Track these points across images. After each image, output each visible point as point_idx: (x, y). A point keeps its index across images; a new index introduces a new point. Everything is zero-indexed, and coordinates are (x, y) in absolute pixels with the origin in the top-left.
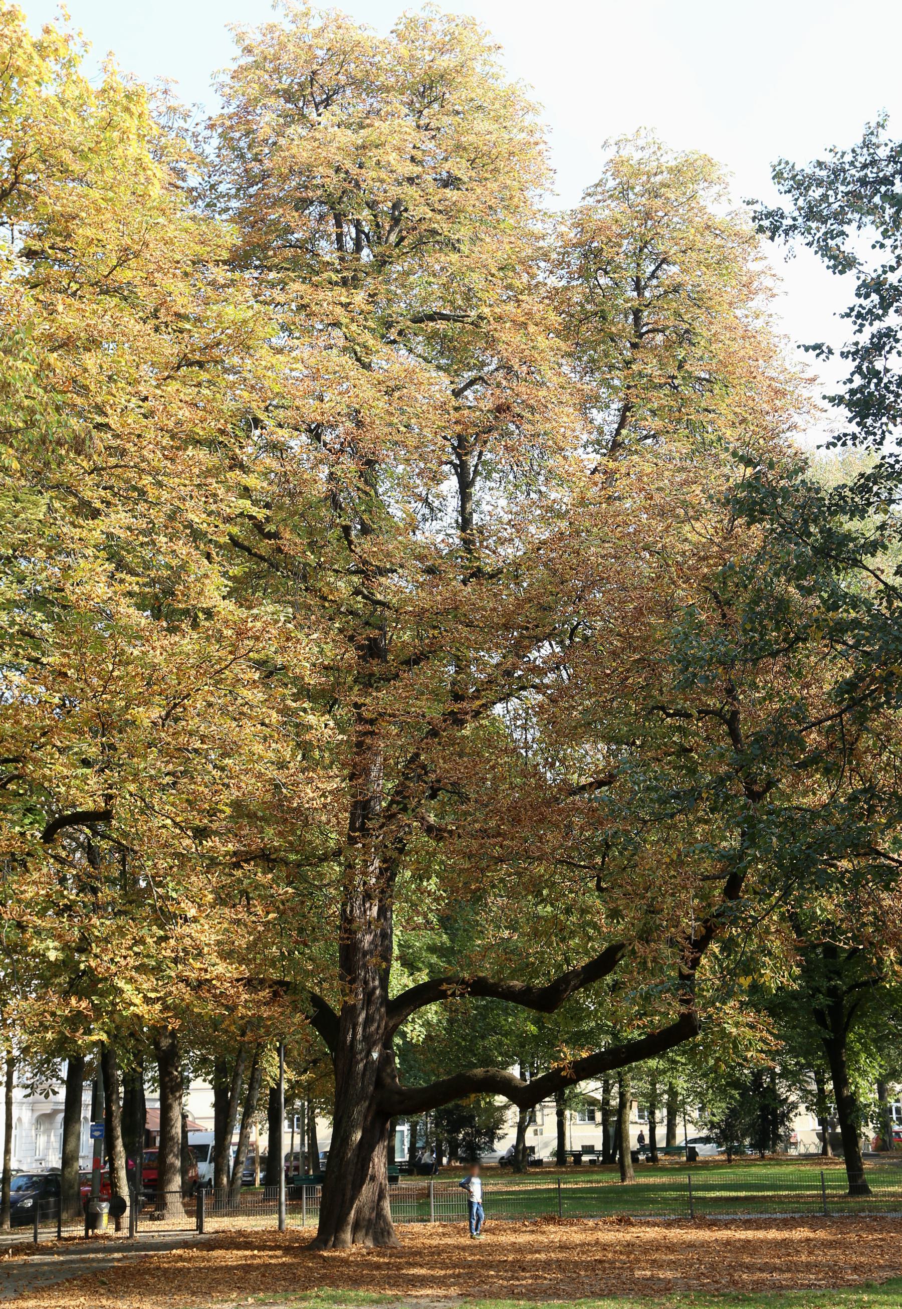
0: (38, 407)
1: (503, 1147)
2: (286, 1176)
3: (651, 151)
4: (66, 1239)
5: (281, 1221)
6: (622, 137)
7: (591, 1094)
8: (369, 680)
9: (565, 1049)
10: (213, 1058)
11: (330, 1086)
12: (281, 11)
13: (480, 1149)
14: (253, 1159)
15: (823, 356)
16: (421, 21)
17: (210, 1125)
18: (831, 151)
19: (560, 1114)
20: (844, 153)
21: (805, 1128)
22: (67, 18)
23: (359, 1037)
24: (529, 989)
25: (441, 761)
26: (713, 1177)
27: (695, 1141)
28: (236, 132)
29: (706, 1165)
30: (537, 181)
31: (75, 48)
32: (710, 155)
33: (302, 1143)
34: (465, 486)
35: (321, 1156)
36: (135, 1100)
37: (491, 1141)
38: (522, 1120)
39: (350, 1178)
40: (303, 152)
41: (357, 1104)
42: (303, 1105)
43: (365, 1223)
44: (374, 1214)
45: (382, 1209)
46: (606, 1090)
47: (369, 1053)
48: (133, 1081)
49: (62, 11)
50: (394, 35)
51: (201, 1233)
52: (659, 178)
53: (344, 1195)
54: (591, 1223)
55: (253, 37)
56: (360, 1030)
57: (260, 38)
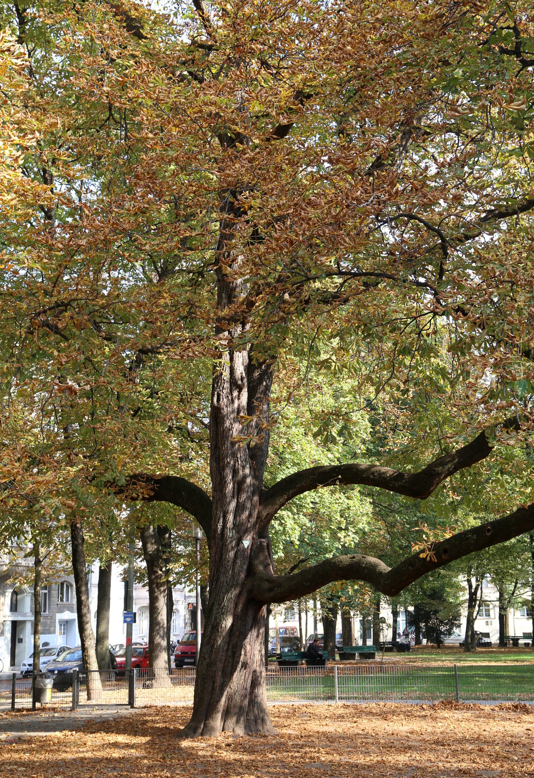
1: (460, 633)
4: (19, 710)
9: (426, 530)
23: (230, 525)
24: (400, 476)
39: (220, 665)
41: (228, 592)
43: (237, 710)
44: (246, 702)
45: (256, 697)
47: (239, 541)
53: (214, 683)
54: (487, 707)
56: (231, 517)
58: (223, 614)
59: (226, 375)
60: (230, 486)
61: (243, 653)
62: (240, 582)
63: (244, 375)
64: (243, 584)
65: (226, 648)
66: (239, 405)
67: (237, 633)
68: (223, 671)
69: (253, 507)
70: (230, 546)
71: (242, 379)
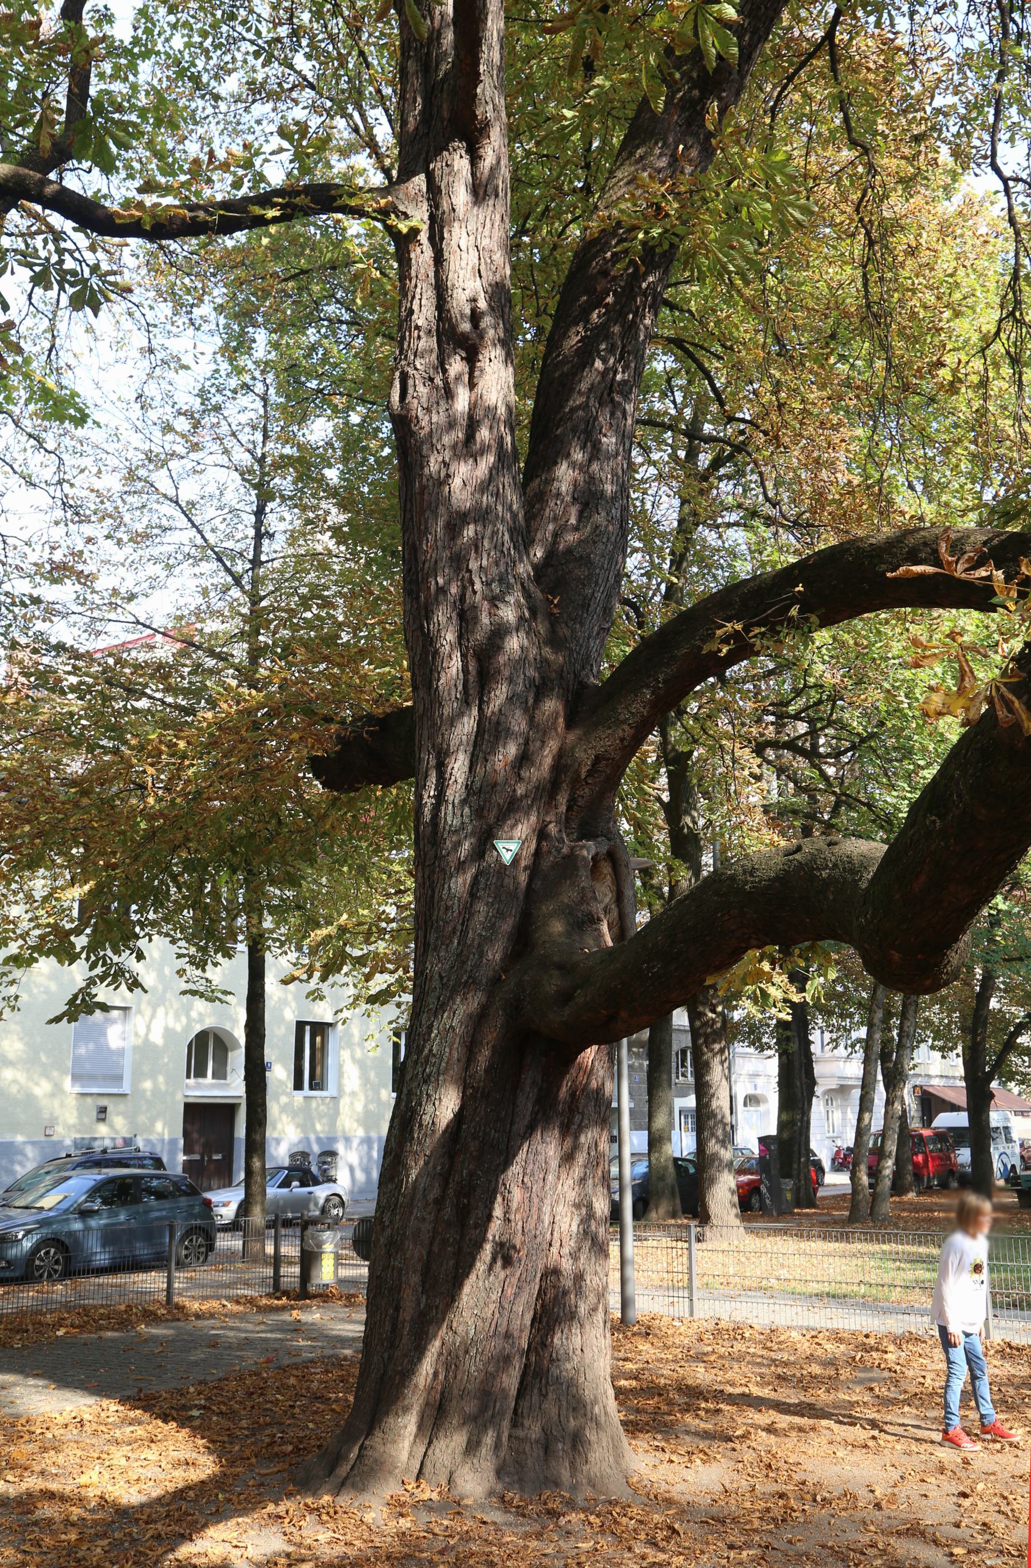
23: (455, 792)
43: (470, 1407)
44: (511, 1380)
47: (485, 840)
53: (397, 1309)
56: (459, 767)
58: (426, 1081)
59: (424, 314)
60: (454, 666)
61: (498, 1211)
62: (484, 974)
63: (482, 304)
64: (495, 982)
65: (434, 1193)
66: (473, 406)
67: (473, 1146)
68: (426, 1272)
69: (538, 730)
70: (452, 859)
71: (475, 317)
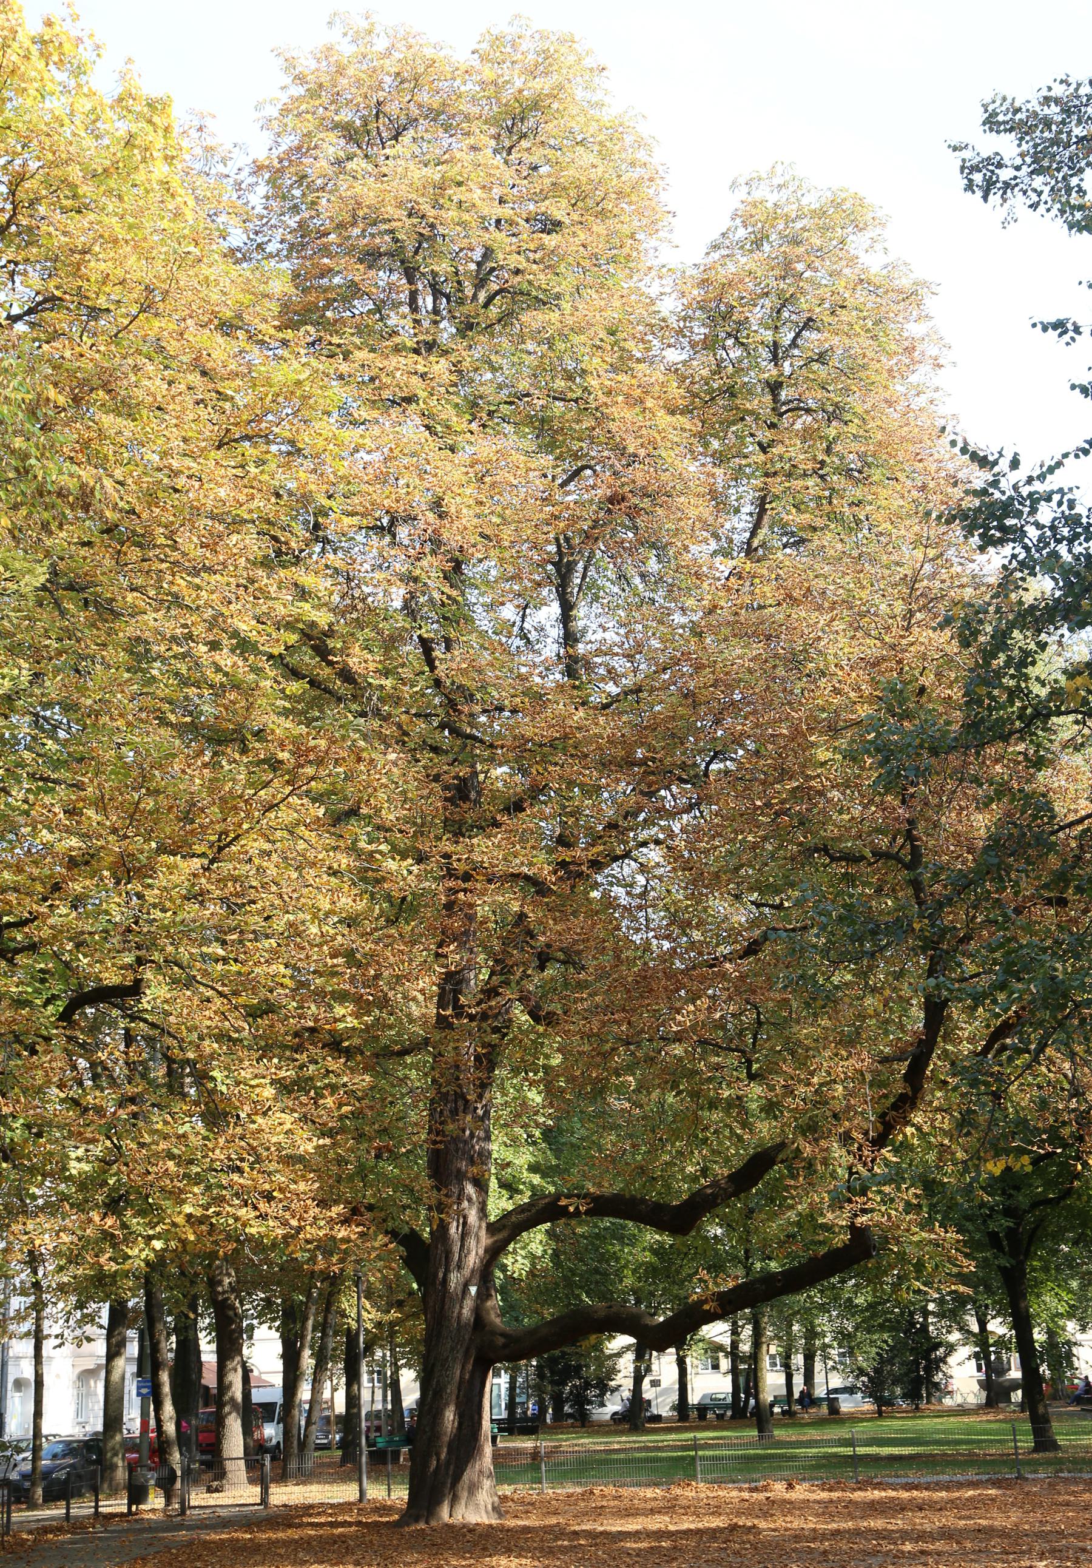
0: (33, 451)
2: (367, 1437)
3: (791, 189)
5: (362, 1492)
6: (755, 175)
7: (716, 1339)
8: (460, 828)
10: (279, 1301)
11: (420, 1326)
12: (338, 29)
13: (590, 1403)
14: (328, 1418)
15: (1066, 338)
16: (509, 38)
17: (278, 1380)
18: (1062, 82)
19: (681, 1363)
20: (1079, 85)
21: (962, 1377)
22: (76, 18)
25: (551, 922)
26: (862, 1429)
27: (836, 1391)
28: (285, 176)
29: (853, 1419)
30: (653, 227)
31: (85, 54)
32: (861, 194)
33: (385, 1400)
34: (567, 608)
35: (406, 1414)
36: (188, 1350)
37: (602, 1395)
38: (637, 1370)
40: (367, 191)
42: (384, 1355)
46: (735, 1332)
48: (186, 1328)
49: (70, 10)
50: (476, 56)
51: (266, 1507)
52: (799, 225)
55: (305, 63)
57: (313, 65)
